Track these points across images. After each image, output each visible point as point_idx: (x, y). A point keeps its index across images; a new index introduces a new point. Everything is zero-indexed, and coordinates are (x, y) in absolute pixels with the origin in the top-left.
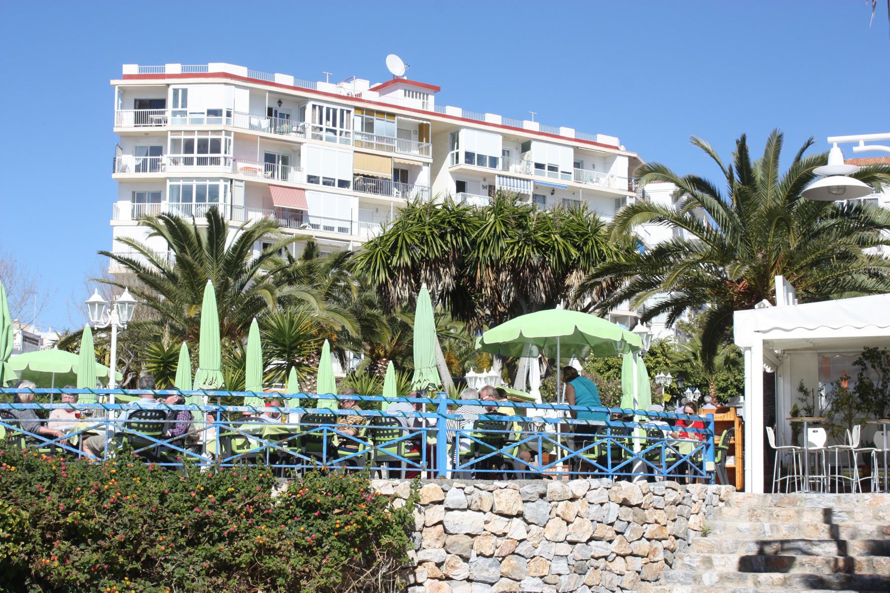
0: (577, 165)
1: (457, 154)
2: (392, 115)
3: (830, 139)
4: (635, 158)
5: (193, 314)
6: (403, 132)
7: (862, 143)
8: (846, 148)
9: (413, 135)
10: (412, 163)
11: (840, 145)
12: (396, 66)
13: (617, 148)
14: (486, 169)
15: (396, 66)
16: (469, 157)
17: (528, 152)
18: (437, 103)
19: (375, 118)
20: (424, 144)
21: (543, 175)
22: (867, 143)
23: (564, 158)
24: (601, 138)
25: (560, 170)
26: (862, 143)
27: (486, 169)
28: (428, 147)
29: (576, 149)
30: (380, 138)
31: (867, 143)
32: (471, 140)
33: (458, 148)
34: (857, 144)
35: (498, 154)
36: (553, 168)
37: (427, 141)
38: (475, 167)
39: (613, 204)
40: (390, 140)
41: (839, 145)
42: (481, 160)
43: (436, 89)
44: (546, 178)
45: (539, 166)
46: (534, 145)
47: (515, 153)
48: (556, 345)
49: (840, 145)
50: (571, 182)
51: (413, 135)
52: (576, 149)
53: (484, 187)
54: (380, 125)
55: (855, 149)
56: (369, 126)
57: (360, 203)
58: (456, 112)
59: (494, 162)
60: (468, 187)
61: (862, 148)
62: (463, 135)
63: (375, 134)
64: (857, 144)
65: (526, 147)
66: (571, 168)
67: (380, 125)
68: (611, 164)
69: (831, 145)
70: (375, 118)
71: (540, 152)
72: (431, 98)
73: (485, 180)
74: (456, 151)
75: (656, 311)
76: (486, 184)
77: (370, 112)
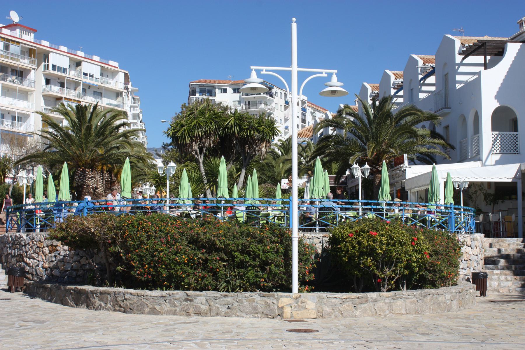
0: (102, 75)
1: (48, 65)
2: (19, 43)
3: (252, 67)
4: (127, 74)
5: (229, 166)
6: (23, 53)
7: (264, 70)
8: (258, 72)
9: (26, 53)
10: (25, 67)
11: (255, 70)
12: (15, 17)
13: (117, 68)
14: (61, 74)
15: (15, 17)
16: (54, 67)
17: (79, 67)
18: (35, 38)
19: (10, 43)
20: (32, 59)
21: (87, 79)
22: (266, 71)
23: (96, 71)
24: (111, 63)
25: (94, 77)
26: (264, 70)
27: (61, 74)
28: (35, 61)
29: (102, 67)
30: (12, 54)
31: (266, 71)
32: (54, 59)
33: (48, 62)
34: (262, 70)
35: (67, 67)
36: (91, 76)
37: (34, 57)
38: (56, 73)
39: (115, 95)
40: (18, 56)
41: (255, 70)
42: (59, 69)
43: (35, 31)
44: (88, 80)
45: (85, 74)
46: (83, 63)
47: (73, 67)
48: (358, 185)
49: (255, 70)
50: (99, 84)
51: (26, 53)
52: (102, 67)
53: (58, 83)
54: (12, 47)
55: (262, 72)
56: (7, 47)
57: (2, 87)
58: (45, 43)
59: (65, 70)
60: (51, 81)
61: (264, 72)
62: (51, 55)
63: (10, 52)
64: (262, 70)
65: (78, 64)
66: (99, 76)
67: (12, 47)
68: (116, 75)
69: (252, 70)
70: (10, 43)
71: (86, 67)
72: (32, 35)
73: (59, 79)
74: (47, 63)
75: (62, 147)
76: (59, 81)
77: (8, 40)
